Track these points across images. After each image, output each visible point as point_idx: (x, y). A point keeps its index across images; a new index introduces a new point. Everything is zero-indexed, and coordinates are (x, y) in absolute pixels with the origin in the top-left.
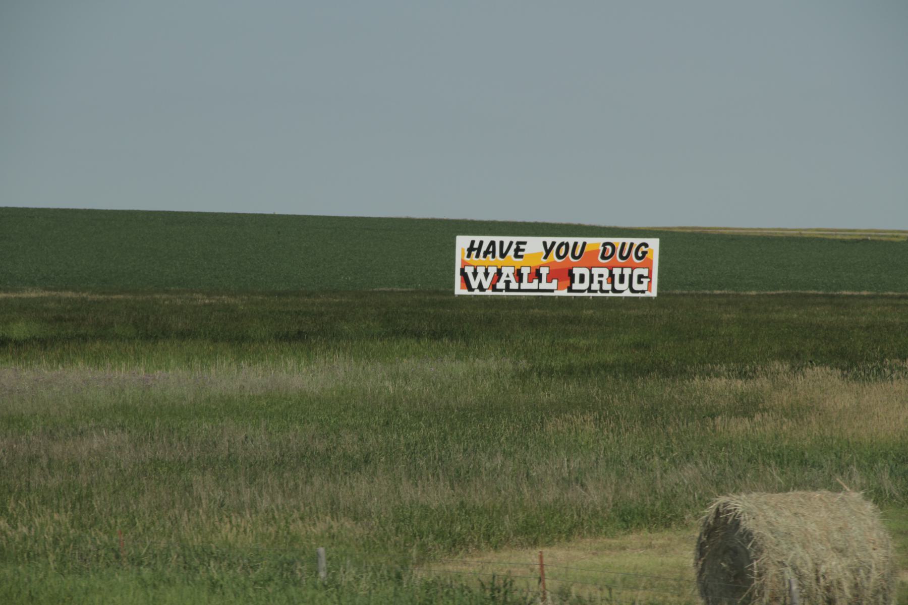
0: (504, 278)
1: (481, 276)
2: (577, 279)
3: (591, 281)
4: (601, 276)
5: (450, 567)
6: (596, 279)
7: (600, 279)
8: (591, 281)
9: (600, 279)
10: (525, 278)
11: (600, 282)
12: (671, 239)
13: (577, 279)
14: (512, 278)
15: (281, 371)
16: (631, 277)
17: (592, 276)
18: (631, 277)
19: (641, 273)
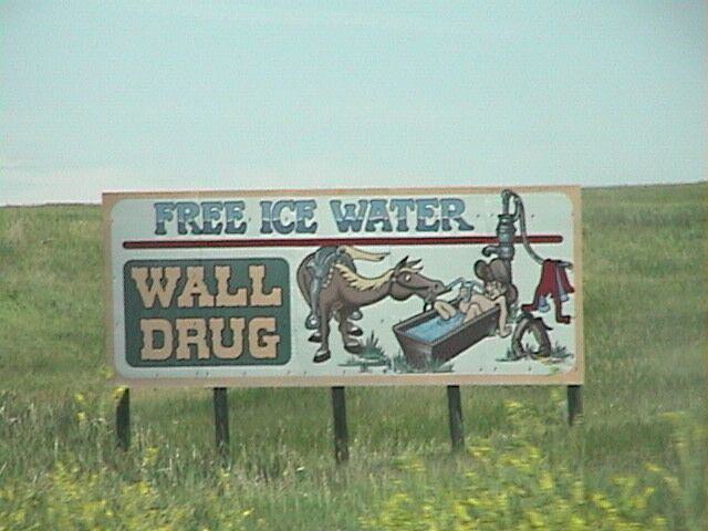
0: (189, 289)
1: (157, 286)
2: (148, 339)
3: (176, 344)
4: (193, 333)
5: (677, 205)
6: (184, 339)
7: (192, 340)
8: (176, 344)
9: (192, 340)
10: (223, 286)
11: (193, 346)
12: (589, 195)
13: (148, 339)
14: (202, 288)
15: (225, 466)
16: (245, 332)
17: (176, 333)
18: (245, 332)
19: (262, 326)
